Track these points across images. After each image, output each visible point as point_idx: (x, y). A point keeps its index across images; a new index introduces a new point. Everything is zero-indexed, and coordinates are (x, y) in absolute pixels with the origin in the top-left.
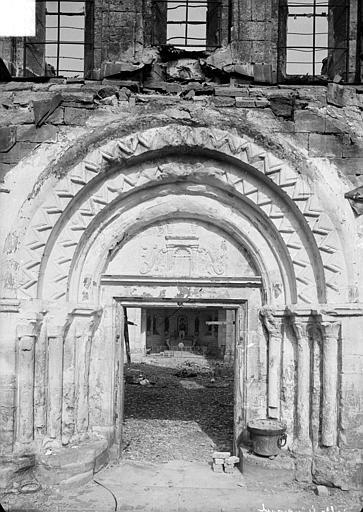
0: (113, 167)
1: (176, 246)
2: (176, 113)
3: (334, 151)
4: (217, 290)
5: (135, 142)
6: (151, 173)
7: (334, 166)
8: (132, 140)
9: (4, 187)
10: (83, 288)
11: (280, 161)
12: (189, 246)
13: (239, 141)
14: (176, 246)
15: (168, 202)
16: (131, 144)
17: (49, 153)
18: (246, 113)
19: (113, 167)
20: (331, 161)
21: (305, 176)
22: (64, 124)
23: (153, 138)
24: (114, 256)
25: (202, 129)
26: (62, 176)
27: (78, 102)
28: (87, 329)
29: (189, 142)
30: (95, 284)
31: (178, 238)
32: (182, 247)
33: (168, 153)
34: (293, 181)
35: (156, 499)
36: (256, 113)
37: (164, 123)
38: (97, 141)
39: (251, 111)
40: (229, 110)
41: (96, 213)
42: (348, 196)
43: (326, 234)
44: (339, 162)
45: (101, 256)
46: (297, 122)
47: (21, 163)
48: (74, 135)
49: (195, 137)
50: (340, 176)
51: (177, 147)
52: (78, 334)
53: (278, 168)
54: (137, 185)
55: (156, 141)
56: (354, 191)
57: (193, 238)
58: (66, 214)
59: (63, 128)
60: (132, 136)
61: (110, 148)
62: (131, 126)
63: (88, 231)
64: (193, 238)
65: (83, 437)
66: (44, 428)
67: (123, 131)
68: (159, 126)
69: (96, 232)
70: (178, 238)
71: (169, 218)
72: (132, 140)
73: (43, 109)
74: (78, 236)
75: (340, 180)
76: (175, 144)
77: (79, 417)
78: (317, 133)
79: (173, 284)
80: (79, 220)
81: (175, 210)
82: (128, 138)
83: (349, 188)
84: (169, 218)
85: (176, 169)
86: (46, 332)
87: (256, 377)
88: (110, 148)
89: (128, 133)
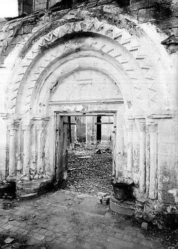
0: (44, 49)
1: (81, 85)
2: (69, 17)
3: (154, 17)
4: (101, 106)
5: (52, 36)
6: (62, 49)
7: (154, 27)
8: (50, 35)
9: (3, 66)
10: (39, 108)
11: (120, 30)
12: (87, 84)
13: (98, 23)
14: (81, 85)
15: (73, 62)
16: (49, 38)
17: (18, 48)
18: (102, 7)
19: (44, 49)
20: (152, 23)
21: (135, 36)
22: (24, 34)
23: (59, 32)
24: (54, 93)
25: (81, 22)
26: (23, 57)
27: (29, 22)
28: (41, 127)
29: (76, 30)
30: (44, 105)
31: (82, 80)
32: (84, 84)
33: (67, 38)
34: (129, 40)
35: (177, 198)
36: (108, 6)
37: (63, 23)
38: (35, 38)
39: (105, 6)
40: (94, 8)
41: (41, 72)
42: (164, 43)
43: (148, 69)
44: (157, 23)
45: (47, 92)
46: (131, 5)
47: (9, 54)
48: (27, 38)
49: (78, 27)
50: (158, 32)
51: (71, 34)
52: (37, 129)
53: (120, 35)
54: (57, 56)
55: (60, 33)
56: (167, 39)
57: (89, 80)
58: (28, 72)
59: (24, 36)
60: (50, 33)
61: (40, 42)
62: (48, 28)
63: (38, 81)
64: (89, 80)
65: (40, 177)
66: (21, 171)
67: (45, 31)
68: (61, 25)
69: (43, 81)
70: (82, 80)
71: (79, 70)
72: (50, 35)
73: (16, 29)
74: (33, 84)
75: (158, 34)
76: (69, 33)
77: (38, 167)
78: (143, 8)
79: (80, 104)
80: (34, 77)
81: (78, 66)
82: (48, 34)
83: (164, 37)
84: (79, 70)
85: (72, 45)
86: (36, 127)
87: (122, 154)
88: (40, 42)
89: (48, 32)
